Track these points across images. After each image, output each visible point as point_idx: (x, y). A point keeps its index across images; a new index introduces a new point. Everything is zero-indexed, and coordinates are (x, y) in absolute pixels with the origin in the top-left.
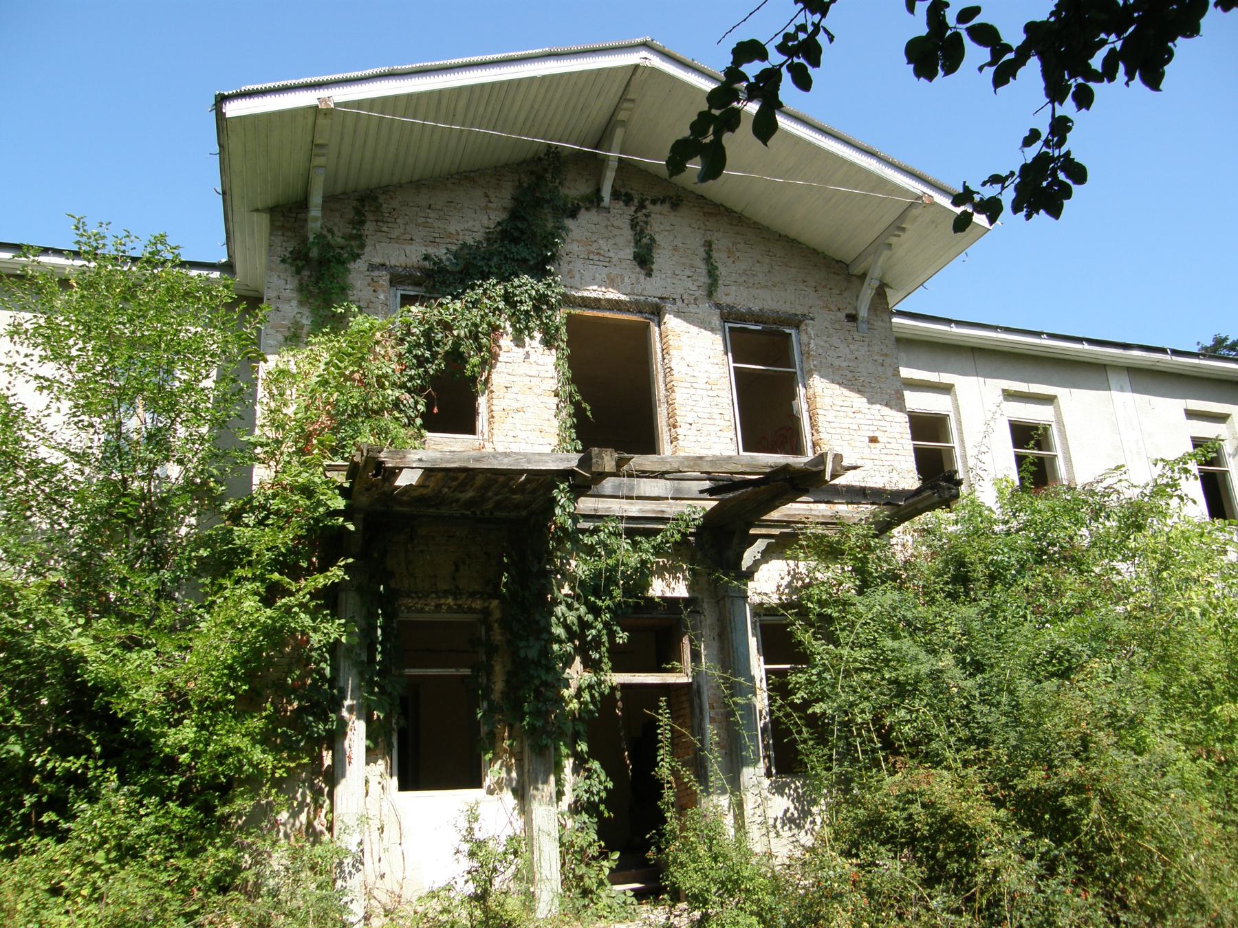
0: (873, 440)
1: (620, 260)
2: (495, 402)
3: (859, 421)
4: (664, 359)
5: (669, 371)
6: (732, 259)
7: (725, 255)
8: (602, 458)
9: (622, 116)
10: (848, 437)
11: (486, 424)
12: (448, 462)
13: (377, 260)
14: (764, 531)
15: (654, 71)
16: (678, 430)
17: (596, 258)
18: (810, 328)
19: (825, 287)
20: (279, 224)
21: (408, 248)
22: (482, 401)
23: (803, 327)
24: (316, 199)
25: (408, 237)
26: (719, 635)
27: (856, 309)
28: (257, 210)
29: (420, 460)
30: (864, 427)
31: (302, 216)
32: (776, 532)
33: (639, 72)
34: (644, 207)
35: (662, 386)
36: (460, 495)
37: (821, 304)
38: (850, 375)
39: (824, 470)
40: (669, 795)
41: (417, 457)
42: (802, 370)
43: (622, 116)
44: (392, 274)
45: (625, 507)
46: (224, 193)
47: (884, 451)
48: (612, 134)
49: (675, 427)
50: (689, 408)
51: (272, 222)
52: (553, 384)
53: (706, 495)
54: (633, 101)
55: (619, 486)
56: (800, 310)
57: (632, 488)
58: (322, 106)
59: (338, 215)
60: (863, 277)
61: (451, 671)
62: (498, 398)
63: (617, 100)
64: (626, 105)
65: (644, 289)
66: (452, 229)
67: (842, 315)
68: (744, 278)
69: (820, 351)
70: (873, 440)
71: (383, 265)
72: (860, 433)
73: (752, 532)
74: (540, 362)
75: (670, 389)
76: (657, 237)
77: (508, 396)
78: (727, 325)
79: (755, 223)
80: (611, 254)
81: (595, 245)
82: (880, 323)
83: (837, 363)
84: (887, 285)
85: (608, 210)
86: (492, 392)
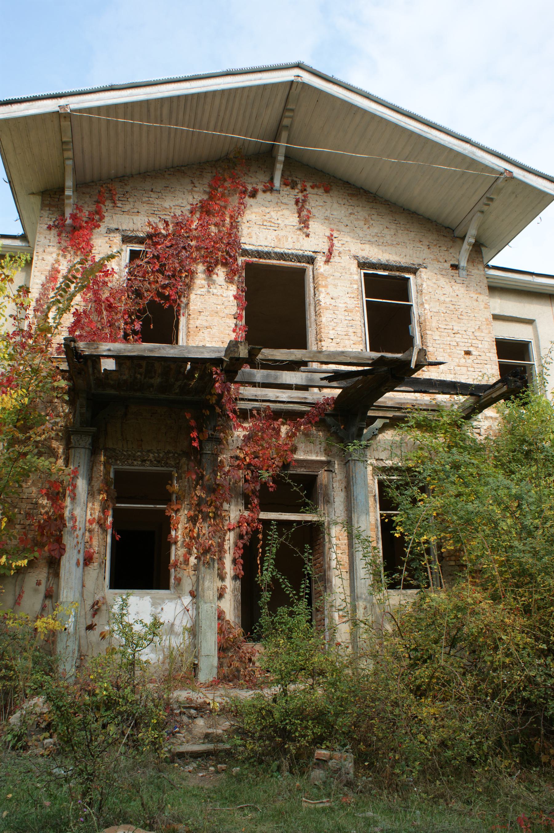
0: (468, 353)
1: (286, 226)
2: (191, 322)
3: (458, 340)
4: (315, 295)
5: (317, 303)
6: (367, 226)
7: (363, 223)
8: (238, 347)
9: (286, 122)
10: (449, 351)
11: (185, 337)
12: (129, 351)
13: (113, 226)
14: (381, 414)
15: (304, 85)
16: (323, 343)
17: (269, 224)
18: (423, 273)
19: (436, 245)
20: (47, 202)
21: (135, 218)
22: (183, 321)
23: (418, 273)
24: (69, 183)
25: (136, 210)
26: (345, 488)
27: (458, 260)
28: (33, 194)
29: (109, 350)
30: (460, 344)
31: (61, 197)
32: (390, 414)
33: (294, 86)
34: (305, 190)
35: (313, 313)
36: (152, 381)
37: (432, 257)
38: (452, 307)
39: (411, 361)
40: (266, 596)
41: (107, 348)
42: (417, 303)
43: (286, 122)
44: (123, 236)
45: (278, 394)
46: (10, 182)
47: (476, 361)
48: (280, 134)
49: (321, 341)
50: (331, 328)
51: (43, 200)
52: (234, 310)
53: (325, 383)
54: (292, 110)
55: (268, 376)
56: (417, 261)
57: (276, 378)
58: (62, 111)
59: (88, 196)
60: (463, 238)
61: (158, 506)
62: (193, 318)
63: (281, 110)
64: (287, 114)
65: (302, 246)
66: (166, 205)
67: (447, 265)
68: (376, 239)
69: (430, 290)
70: (468, 353)
71: (117, 229)
72: (458, 348)
73: (370, 413)
74: (224, 295)
75: (318, 314)
76: (313, 211)
77: (200, 318)
78: (363, 271)
79: (386, 201)
80: (279, 222)
81: (268, 216)
82: (476, 271)
83: (442, 298)
84: (482, 245)
85: (278, 191)
86: (189, 315)
